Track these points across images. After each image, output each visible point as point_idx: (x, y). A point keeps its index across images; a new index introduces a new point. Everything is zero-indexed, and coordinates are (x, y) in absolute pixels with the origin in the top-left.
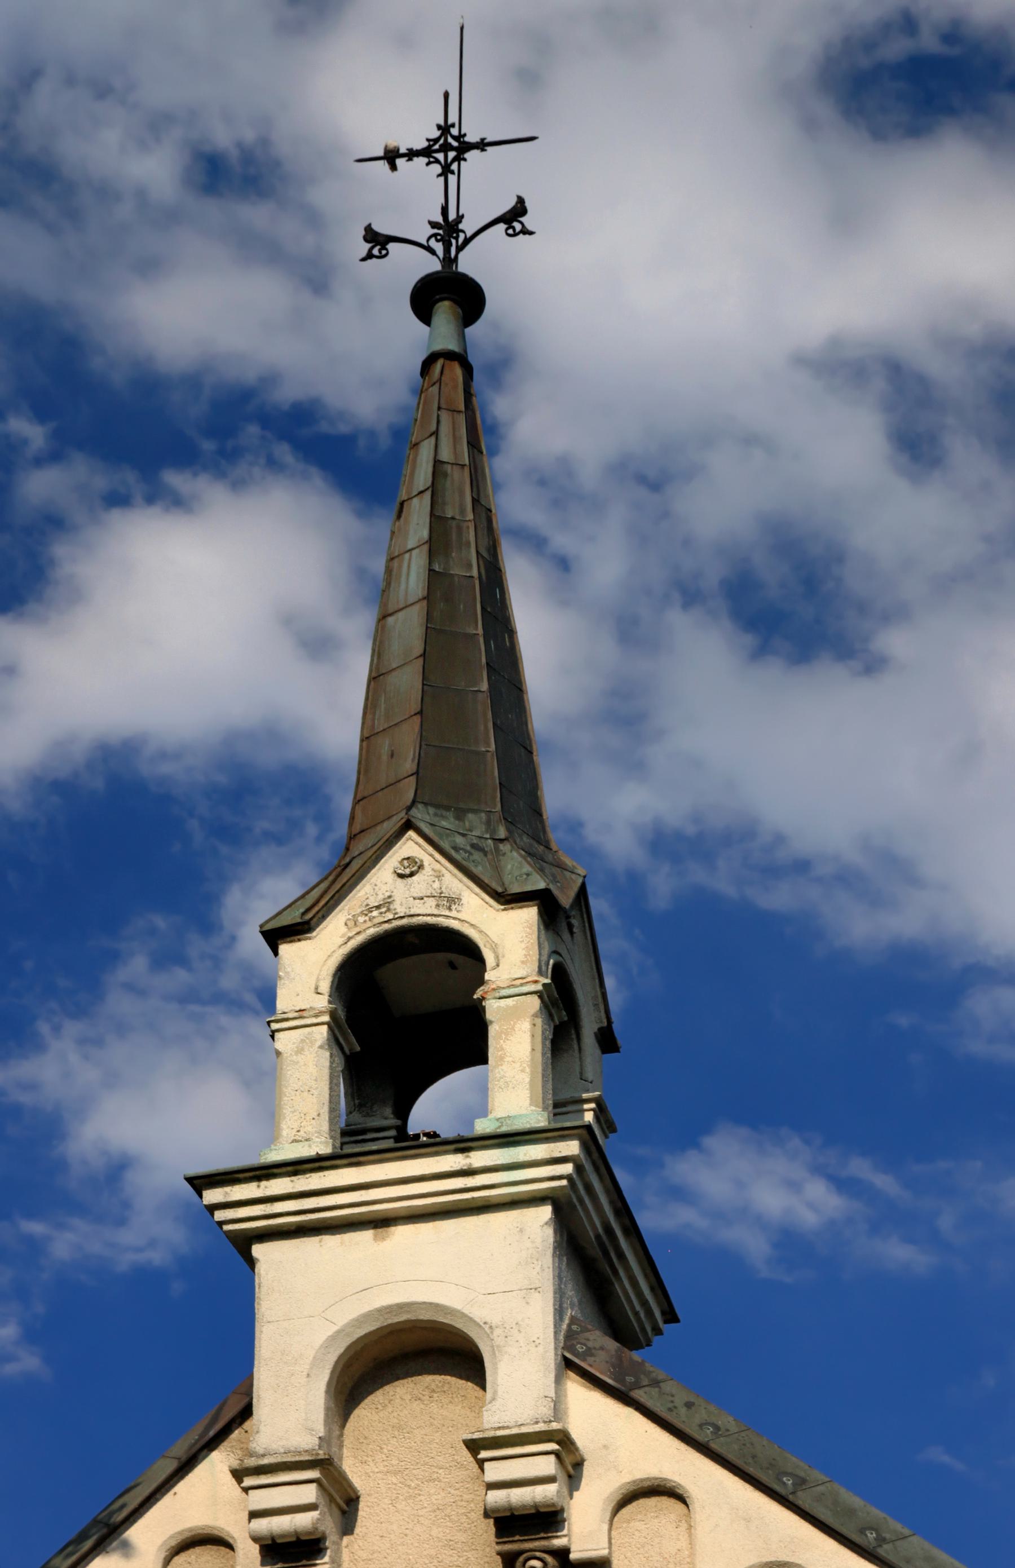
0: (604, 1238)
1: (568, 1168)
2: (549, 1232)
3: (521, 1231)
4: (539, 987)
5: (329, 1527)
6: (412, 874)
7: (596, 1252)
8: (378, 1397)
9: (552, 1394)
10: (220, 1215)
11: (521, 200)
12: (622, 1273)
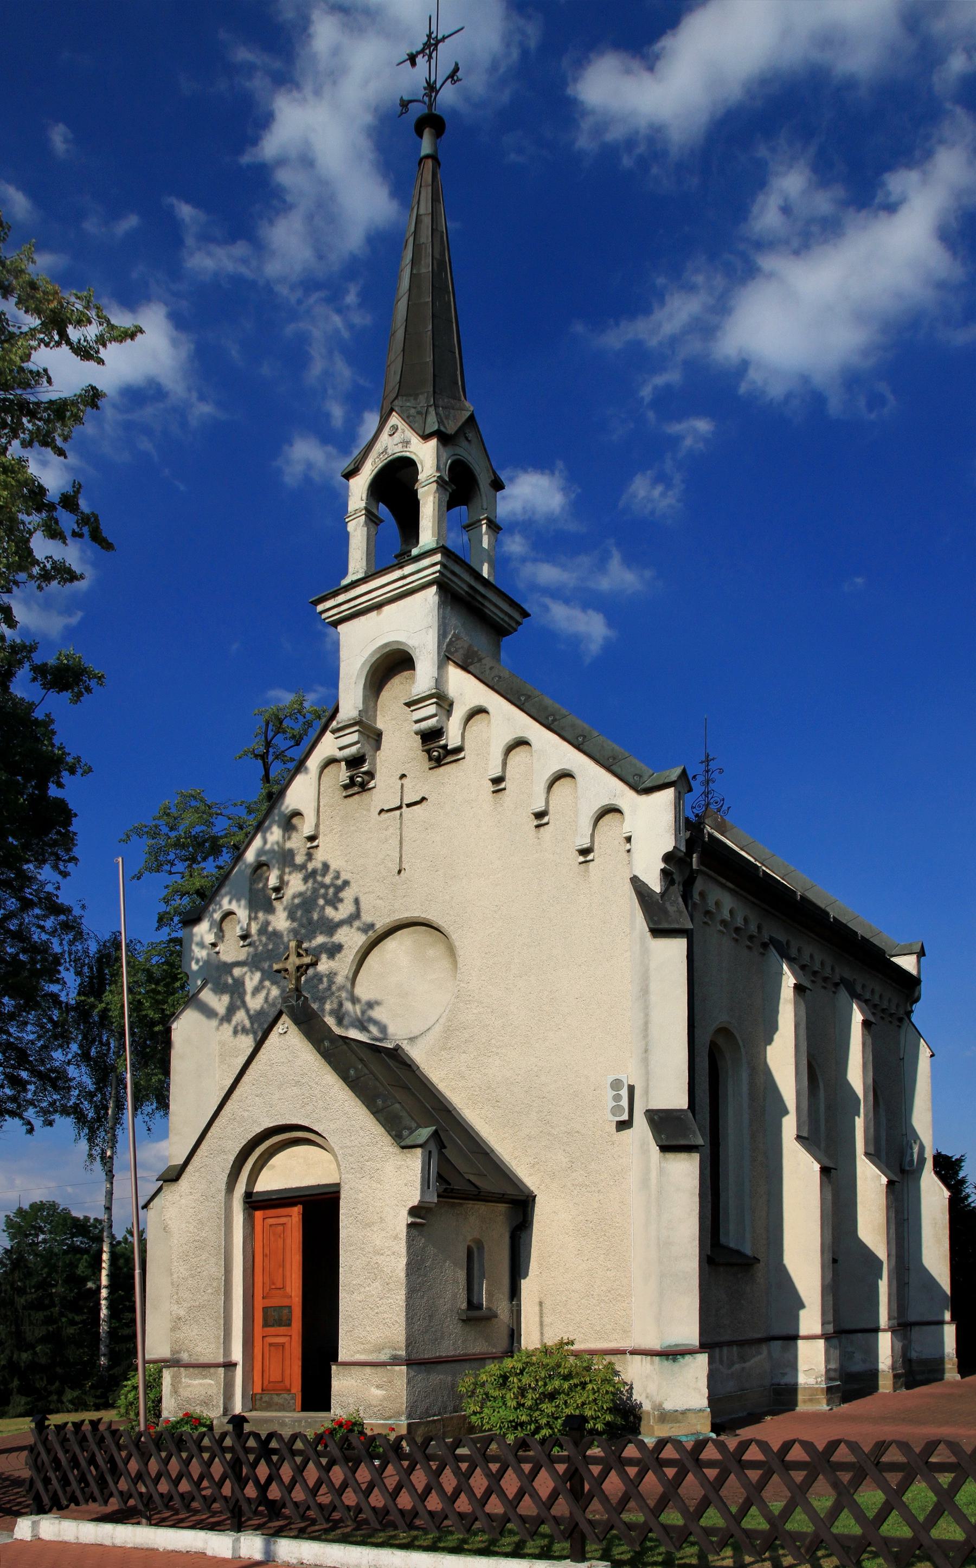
0: (470, 591)
1: (438, 567)
2: (437, 598)
3: (426, 600)
4: (436, 478)
5: (368, 750)
6: (394, 433)
7: (469, 599)
8: (388, 686)
9: (436, 676)
10: (324, 616)
11: (457, 64)
12: (487, 604)
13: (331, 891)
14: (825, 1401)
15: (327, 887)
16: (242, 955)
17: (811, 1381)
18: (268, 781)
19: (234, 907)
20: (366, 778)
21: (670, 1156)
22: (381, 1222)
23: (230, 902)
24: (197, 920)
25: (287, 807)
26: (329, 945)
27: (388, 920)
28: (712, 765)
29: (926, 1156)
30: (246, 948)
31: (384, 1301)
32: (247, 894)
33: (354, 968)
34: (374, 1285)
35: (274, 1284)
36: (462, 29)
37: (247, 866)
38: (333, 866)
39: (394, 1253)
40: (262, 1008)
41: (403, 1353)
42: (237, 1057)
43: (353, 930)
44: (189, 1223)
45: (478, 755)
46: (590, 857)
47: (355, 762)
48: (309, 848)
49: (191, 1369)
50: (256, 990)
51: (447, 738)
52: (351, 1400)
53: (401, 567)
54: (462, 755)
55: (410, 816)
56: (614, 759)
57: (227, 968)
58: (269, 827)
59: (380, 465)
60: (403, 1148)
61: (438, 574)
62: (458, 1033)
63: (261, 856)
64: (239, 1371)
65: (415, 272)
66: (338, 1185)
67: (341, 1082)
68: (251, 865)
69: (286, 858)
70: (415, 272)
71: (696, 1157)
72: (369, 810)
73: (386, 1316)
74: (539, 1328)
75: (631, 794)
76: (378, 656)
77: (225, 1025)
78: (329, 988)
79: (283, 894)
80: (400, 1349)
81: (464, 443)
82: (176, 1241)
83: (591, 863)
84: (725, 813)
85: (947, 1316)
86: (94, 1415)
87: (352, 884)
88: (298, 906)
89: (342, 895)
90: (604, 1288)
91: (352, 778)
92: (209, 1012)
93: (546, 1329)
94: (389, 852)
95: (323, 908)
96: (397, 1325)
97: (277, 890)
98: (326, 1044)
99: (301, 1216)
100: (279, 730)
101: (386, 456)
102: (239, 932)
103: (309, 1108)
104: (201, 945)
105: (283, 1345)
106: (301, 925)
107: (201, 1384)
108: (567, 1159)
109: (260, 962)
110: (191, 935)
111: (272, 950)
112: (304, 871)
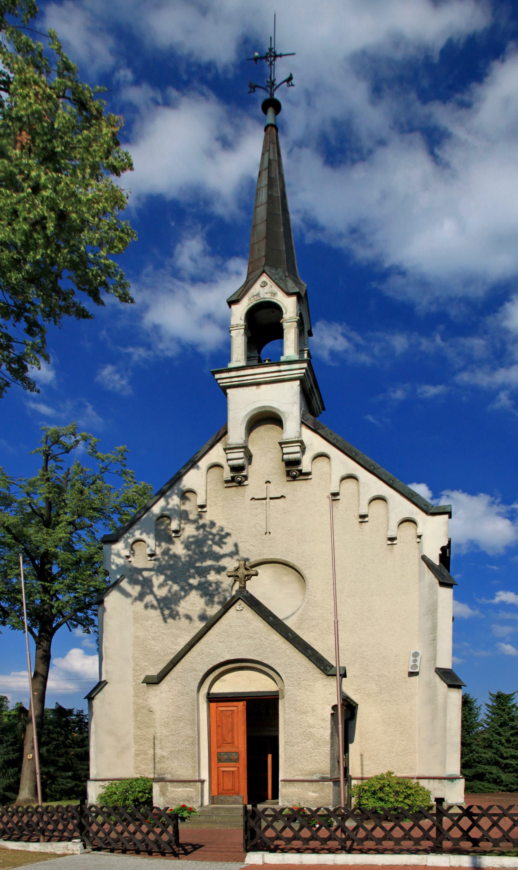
1: (304, 371)
3: (292, 387)
6: (265, 286)
10: (219, 381)
11: (291, 75)
12: (314, 399)
13: (217, 538)
15: (214, 535)
16: (151, 564)
18: (47, 470)
19: (144, 537)
20: (243, 479)
21: (451, 689)
22: (313, 712)
23: (141, 534)
24: (115, 541)
25: (184, 486)
26: (217, 566)
27: (259, 558)
30: (153, 562)
31: (316, 751)
32: (154, 531)
34: (309, 743)
35: (225, 741)
36: (293, 54)
37: (154, 515)
38: (218, 524)
39: (322, 727)
40: (167, 595)
41: (329, 776)
42: (147, 621)
43: (233, 560)
44: (169, 707)
45: (321, 479)
46: (395, 542)
47: (237, 469)
48: (199, 512)
49: (176, 783)
50: (161, 586)
52: (294, 798)
53: (279, 365)
54: (310, 477)
55: (273, 504)
56: (412, 495)
57: (140, 571)
58: (170, 496)
59: (255, 302)
60: (328, 675)
61: (303, 375)
62: (308, 622)
63: (164, 511)
64: (206, 785)
66: (277, 692)
67: (283, 639)
68: (156, 515)
69: (184, 516)
70: (270, 193)
72: (243, 497)
73: (316, 758)
74: (360, 767)
75: (423, 514)
76: (256, 412)
77: (138, 603)
78: (217, 589)
79: (181, 535)
80: (327, 774)
82: (158, 716)
83: (395, 546)
87: (233, 535)
88: (192, 543)
89: (225, 540)
90: (400, 749)
91: (233, 478)
92: (127, 595)
93: (364, 767)
94: (258, 522)
95: (211, 546)
96: (324, 762)
97: (176, 532)
99: (245, 707)
100: (57, 442)
101: (259, 298)
102: (148, 552)
103: (260, 651)
104: (119, 555)
105: (233, 772)
106: (195, 553)
107: (183, 791)
108: (378, 688)
109: (163, 570)
110: (110, 549)
111: (172, 565)
112: (196, 524)
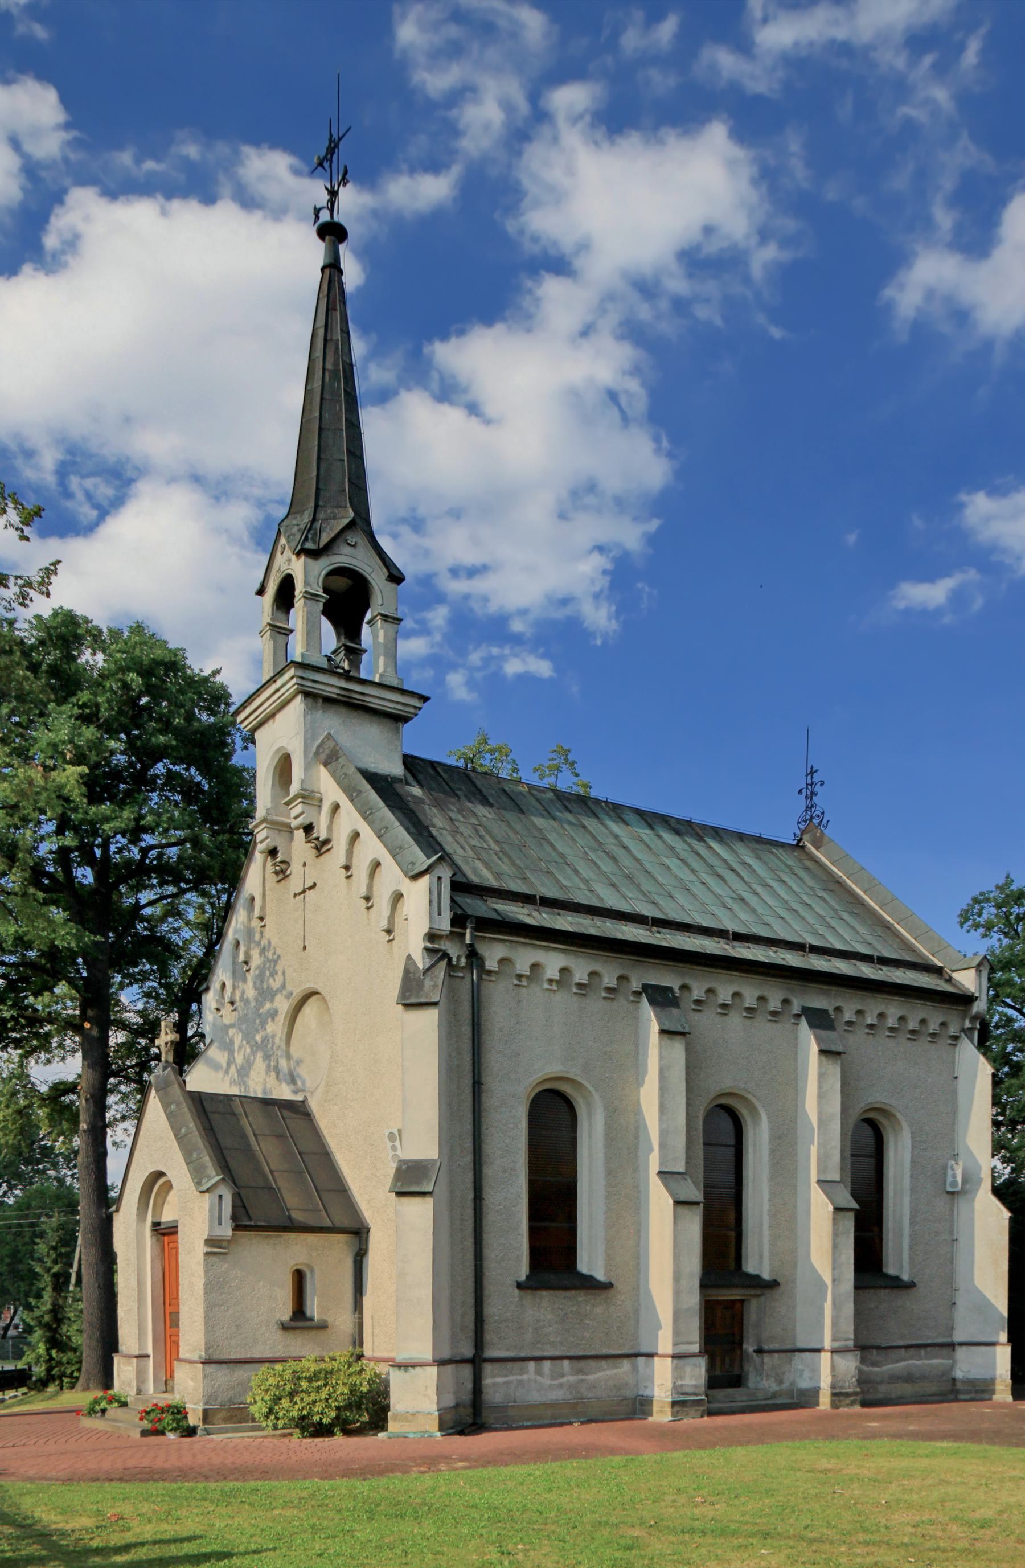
1: (294, 681)
14: (669, 1413)
17: (663, 1395)
20: (283, 866)
21: (405, 1200)
28: (817, 778)
29: (982, 1176)
33: (286, 1030)
51: (319, 831)
54: (329, 846)
65: (309, 388)
66: (177, 1221)
71: (428, 1203)
81: (346, 550)
84: (825, 827)
85: (1003, 1337)
86: (519, 1377)
98: (173, 1107)
